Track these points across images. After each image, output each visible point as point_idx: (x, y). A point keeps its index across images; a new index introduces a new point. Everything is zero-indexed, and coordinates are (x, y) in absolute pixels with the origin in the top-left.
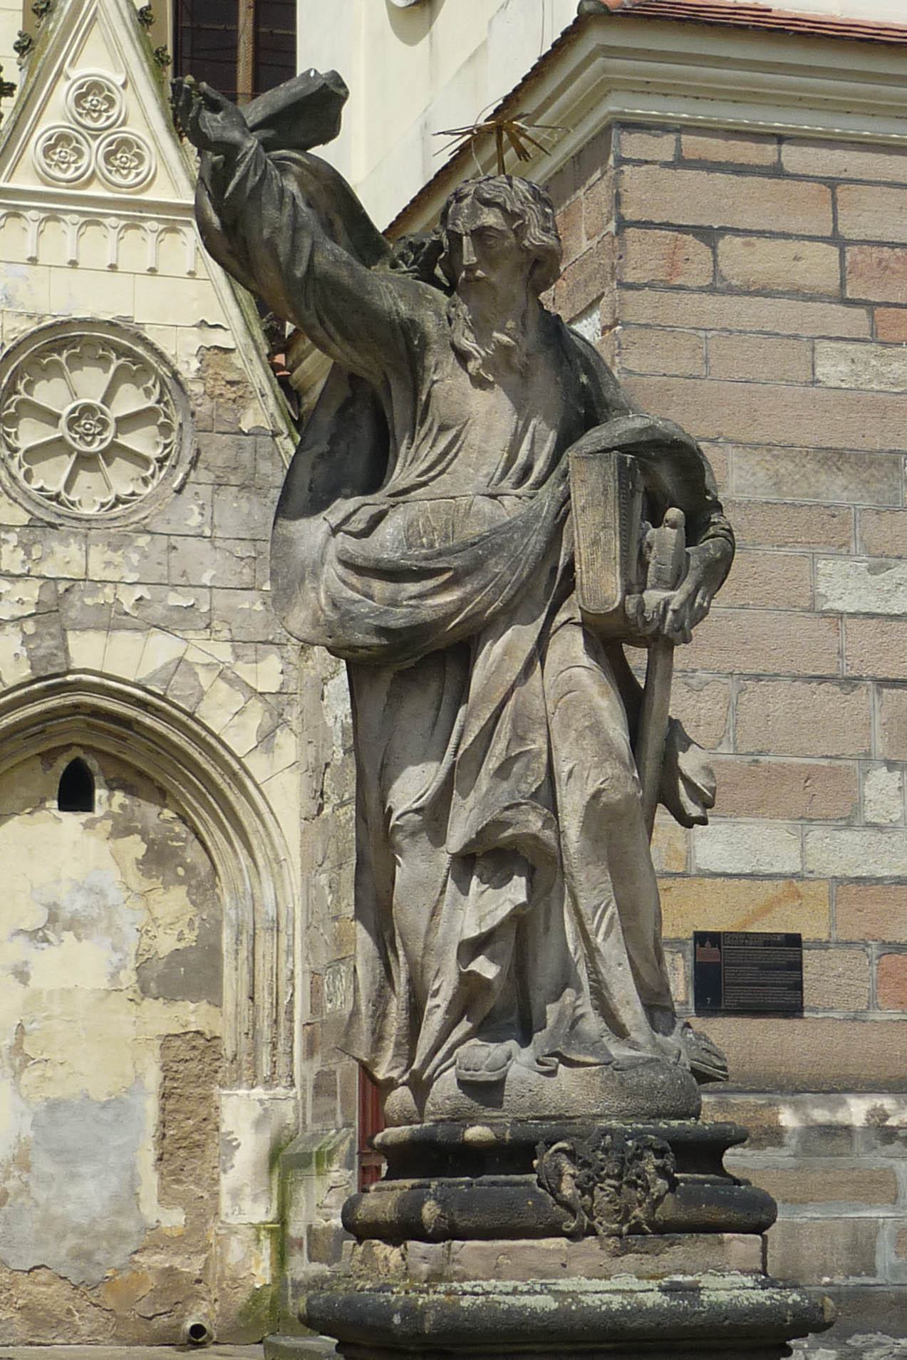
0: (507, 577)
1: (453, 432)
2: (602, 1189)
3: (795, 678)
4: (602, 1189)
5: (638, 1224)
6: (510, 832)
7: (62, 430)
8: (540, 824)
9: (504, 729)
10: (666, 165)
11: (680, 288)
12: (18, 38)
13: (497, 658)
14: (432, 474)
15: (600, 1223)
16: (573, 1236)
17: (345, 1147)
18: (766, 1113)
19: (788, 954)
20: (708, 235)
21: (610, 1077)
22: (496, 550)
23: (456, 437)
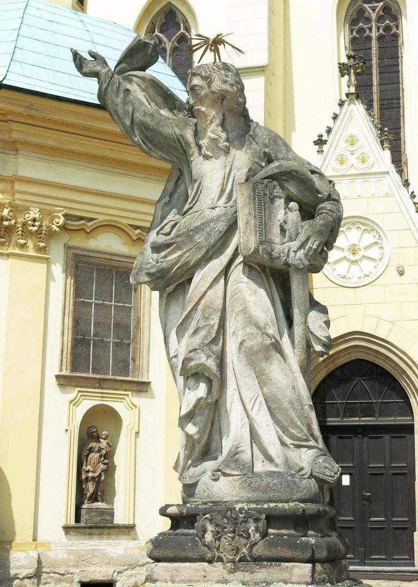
0: (203, 244)
2: (225, 538)
4: (225, 538)
5: (245, 556)
8: (205, 358)
9: (198, 315)
12: (339, 102)
13: (202, 278)
14: (194, 202)
15: (225, 556)
16: (210, 562)
23: (200, 184)
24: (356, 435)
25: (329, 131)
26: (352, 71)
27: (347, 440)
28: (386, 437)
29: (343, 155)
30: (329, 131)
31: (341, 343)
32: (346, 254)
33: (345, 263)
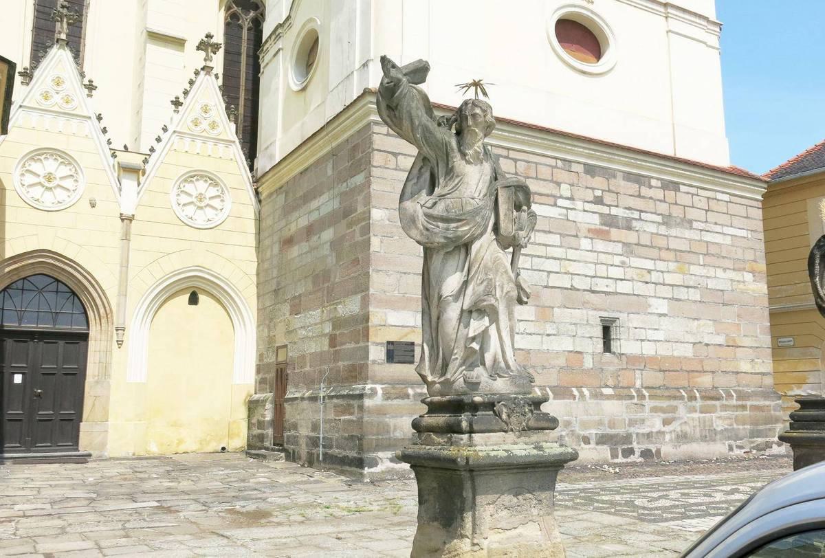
1: (460, 178)
3: (414, 274)
6: (485, 303)
7: (194, 199)
10: (384, 135)
11: (388, 168)
17: (270, 399)
18: (404, 390)
19: (409, 348)
20: (395, 155)
21: (512, 381)
22: (477, 214)
23: (461, 179)
24: (32, 339)
25: (186, 93)
26: (65, 20)
27: (22, 344)
28: (61, 343)
29: (48, 92)
30: (186, 93)
31: (28, 259)
32: (42, 180)
33: (39, 187)
